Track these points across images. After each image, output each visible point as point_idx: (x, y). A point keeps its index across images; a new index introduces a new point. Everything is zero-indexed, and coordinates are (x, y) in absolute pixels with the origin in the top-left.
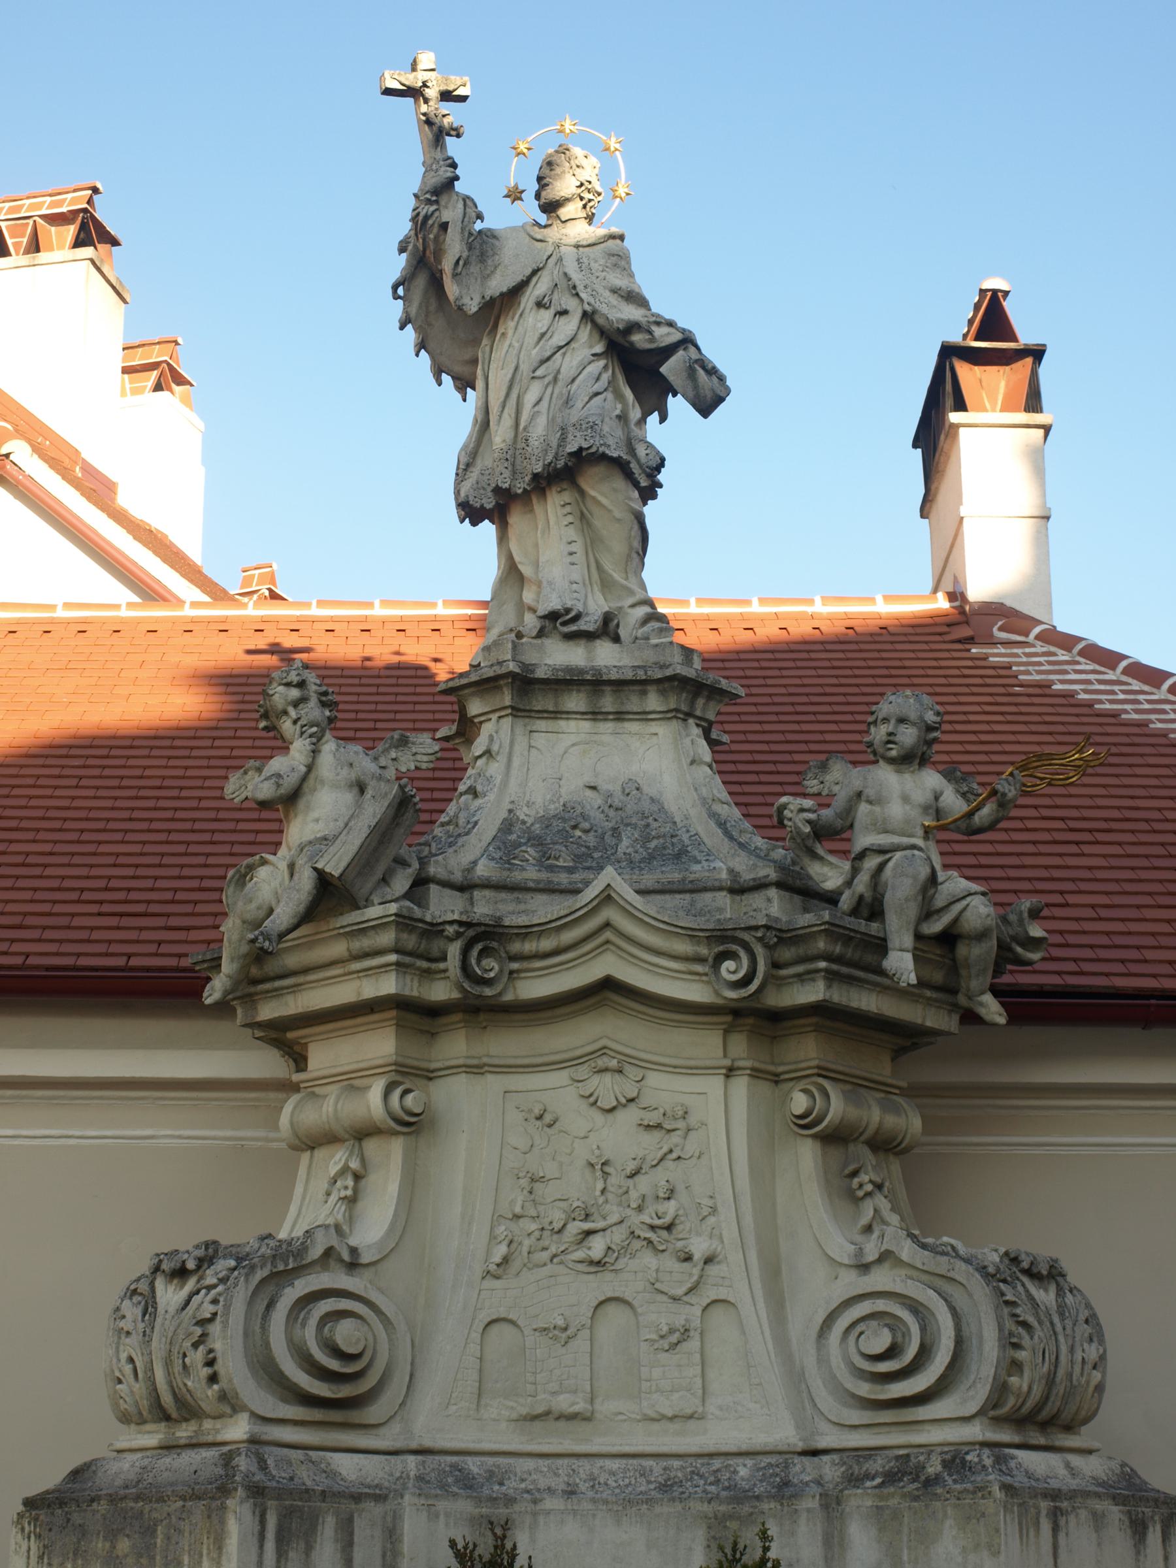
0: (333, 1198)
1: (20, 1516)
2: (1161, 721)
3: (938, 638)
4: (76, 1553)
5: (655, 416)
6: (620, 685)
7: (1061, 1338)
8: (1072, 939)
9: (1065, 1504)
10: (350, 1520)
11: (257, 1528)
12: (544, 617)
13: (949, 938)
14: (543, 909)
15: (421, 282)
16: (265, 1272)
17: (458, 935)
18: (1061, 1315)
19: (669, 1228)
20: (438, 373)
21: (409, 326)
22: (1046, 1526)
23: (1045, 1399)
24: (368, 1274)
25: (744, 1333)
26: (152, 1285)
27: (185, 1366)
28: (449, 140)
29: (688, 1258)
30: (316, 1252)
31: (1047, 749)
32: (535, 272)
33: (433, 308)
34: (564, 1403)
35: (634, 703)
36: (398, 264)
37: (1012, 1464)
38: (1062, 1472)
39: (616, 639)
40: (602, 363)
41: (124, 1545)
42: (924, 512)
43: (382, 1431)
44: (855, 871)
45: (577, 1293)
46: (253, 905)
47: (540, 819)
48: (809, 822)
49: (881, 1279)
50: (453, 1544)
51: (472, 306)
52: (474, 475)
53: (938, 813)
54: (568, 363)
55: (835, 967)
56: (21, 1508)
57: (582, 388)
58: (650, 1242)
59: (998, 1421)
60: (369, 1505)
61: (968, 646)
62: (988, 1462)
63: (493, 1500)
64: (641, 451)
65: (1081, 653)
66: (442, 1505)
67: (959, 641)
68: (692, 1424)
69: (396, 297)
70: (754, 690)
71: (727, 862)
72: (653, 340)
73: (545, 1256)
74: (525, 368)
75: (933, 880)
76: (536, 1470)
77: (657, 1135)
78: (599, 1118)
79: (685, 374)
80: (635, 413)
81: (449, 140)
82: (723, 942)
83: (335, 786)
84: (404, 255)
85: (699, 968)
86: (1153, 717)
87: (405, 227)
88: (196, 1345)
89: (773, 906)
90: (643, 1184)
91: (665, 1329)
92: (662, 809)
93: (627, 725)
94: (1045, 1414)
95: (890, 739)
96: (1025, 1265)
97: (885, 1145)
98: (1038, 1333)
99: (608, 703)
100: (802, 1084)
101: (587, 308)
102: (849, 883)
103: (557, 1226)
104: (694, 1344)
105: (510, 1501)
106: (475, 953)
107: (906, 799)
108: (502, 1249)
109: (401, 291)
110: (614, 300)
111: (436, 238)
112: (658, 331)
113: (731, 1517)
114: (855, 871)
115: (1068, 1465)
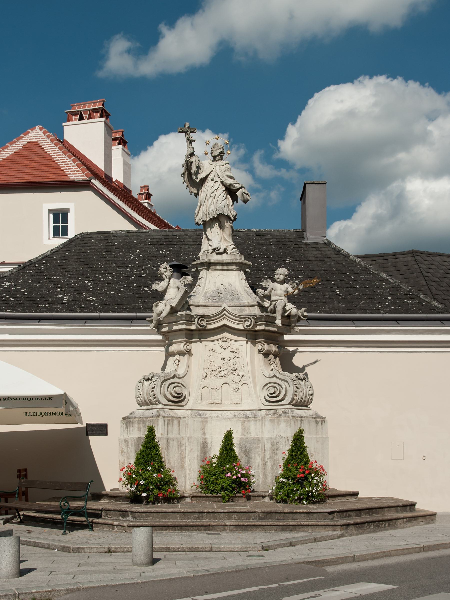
5: (236, 202)
13: (289, 316)
17: (197, 317)
22: (299, 422)
34: (217, 401)
35: (230, 267)
36: (183, 170)
39: (227, 254)
40: (224, 192)
42: (301, 200)
44: (271, 304)
45: (219, 382)
46: (158, 311)
47: (212, 291)
49: (274, 380)
53: (288, 292)
54: (218, 193)
57: (220, 199)
59: (293, 405)
62: (290, 412)
69: (182, 177)
73: (213, 375)
74: (209, 194)
83: (173, 288)
88: (152, 392)
89: (256, 311)
90: (231, 362)
92: (236, 289)
95: (278, 278)
100: (260, 344)
102: (270, 306)
104: (240, 391)
106: (200, 320)
107: (281, 290)
108: (206, 374)
110: (227, 178)
112: (236, 185)
114: (271, 304)
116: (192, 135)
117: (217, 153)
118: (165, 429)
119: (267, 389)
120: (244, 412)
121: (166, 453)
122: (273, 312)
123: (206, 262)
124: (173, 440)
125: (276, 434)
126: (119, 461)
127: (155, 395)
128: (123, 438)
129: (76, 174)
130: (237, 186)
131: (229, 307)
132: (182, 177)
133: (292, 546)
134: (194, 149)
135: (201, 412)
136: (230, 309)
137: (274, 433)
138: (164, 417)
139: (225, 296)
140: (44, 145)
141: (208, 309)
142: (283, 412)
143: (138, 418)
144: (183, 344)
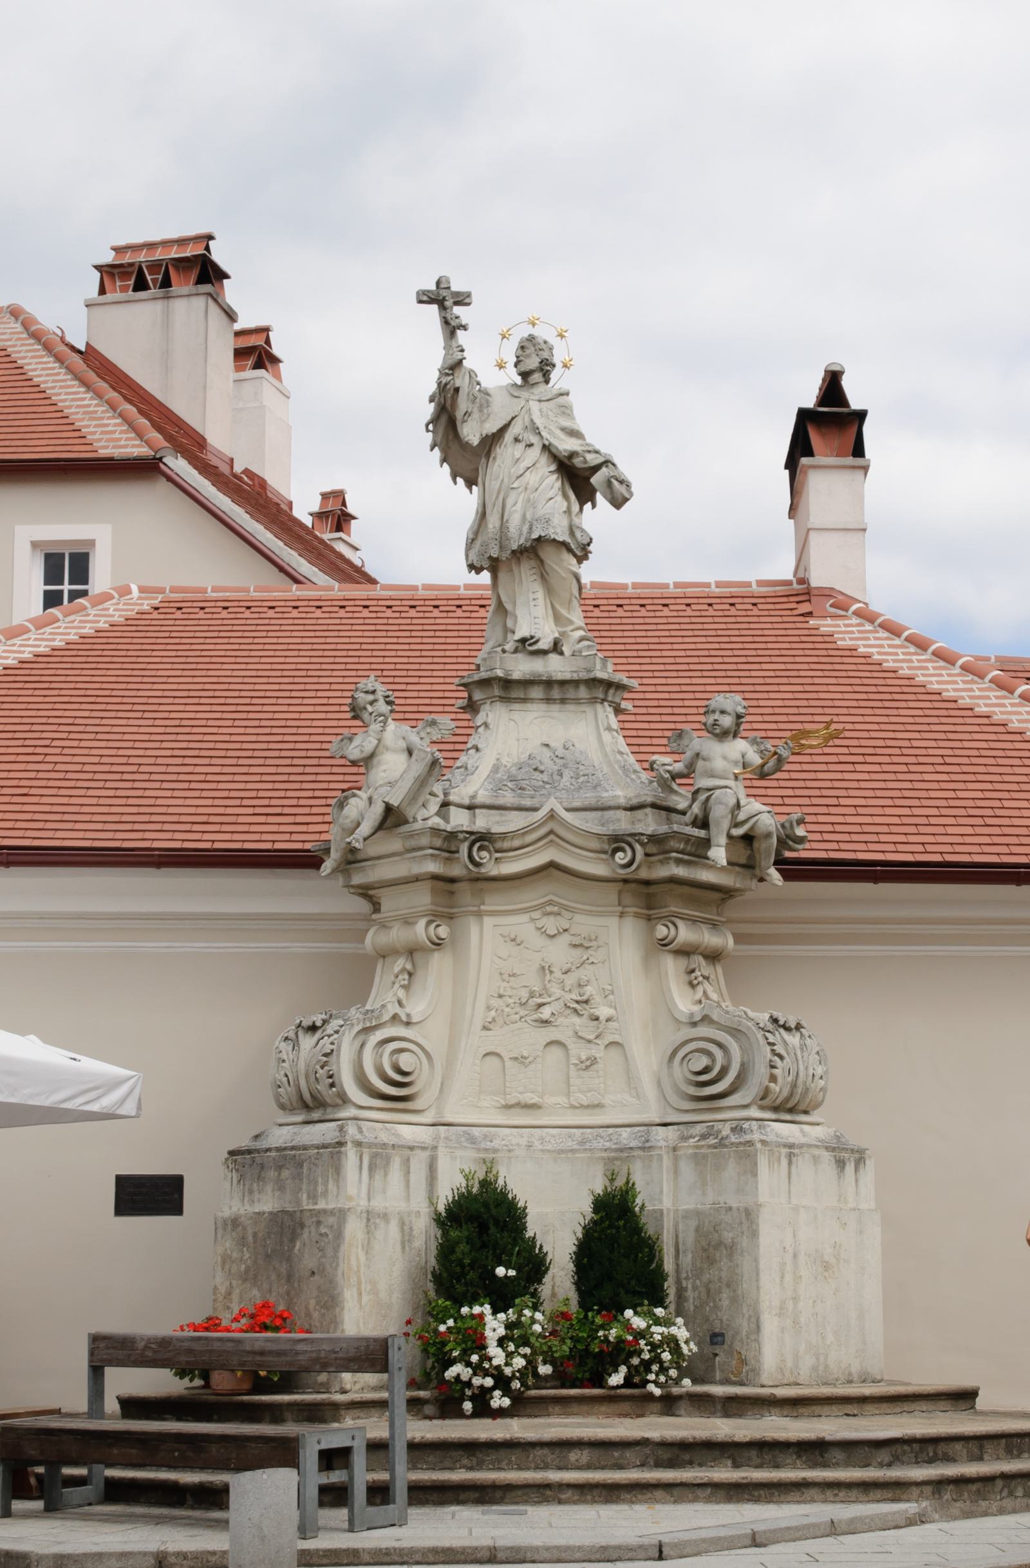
0: (397, 986)
1: (227, 1159)
2: (923, 675)
3: (789, 613)
4: (259, 1178)
5: (589, 505)
6: (563, 683)
7: (800, 1062)
8: (838, 828)
9: (796, 1151)
10: (408, 1160)
11: (358, 1163)
12: (518, 641)
14: (515, 822)
15: (444, 419)
16: (360, 1027)
17: (466, 839)
18: (802, 1049)
19: (586, 1002)
20: (454, 478)
21: (436, 448)
22: (784, 1162)
23: (791, 1094)
24: (417, 1028)
25: (626, 1059)
26: (296, 1034)
27: (316, 1079)
28: (459, 333)
29: (597, 1019)
30: (386, 1017)
31: (808, 727)
32: (513, 418)
33: (451, 437)
35: (571, 693)
36: (429, 409)
37: (768, 1129)
38: (798, 1134)
39: (562, 653)
41: (286, 1173)
43: (426, 1113)
44: (694, 800)
45: (531, 1039)
46: (348, 821)
47: (514, 765)
48: (668, 771)
50: (462, 1171)
51: (475, 441)
52: (477, 545)
54: (532, 478)
55: (680, 856)
56: (227, 1156)
58: (575, 1010)
60: (418, 1152)
61: (807, 619)
63: (486, 1150)
64: (578, 534)
65: (880, 625)
66: (458, 1153)
67: (802, 615)
68: (597, 1110)
69: (428, 431)
70: (645, 681)
71: (621, 794)
72: (585, 461)
73: (518, 1017)
75: (738, 806)
76: (511, 1134)
77: (579, 951)
78: (548, 942)
79: (605, 485)
80: (576, 507)
81: (459, 333)
82: (617, 842)
84: (433, 404)
85: (603, 856)
86: (919, 672)
87: (433, 387)
89: (649, 823)
90: (570, 980)
91: (584, 1058)
93: (567, 706)
94: (790, 1105)
96: (781, 1023)
97: (713, 956)
98: (787, 1059)
99: (556, 693)
101: (547, 443)
102: (690, 806)
103: (524, 1000)
105: (495, 1151)
109: (431, 427)
110: (562, 435)
111: (453, 396)
112: (589, 457)
113: (617, 1159)
115: (802, 1131)
116: (457, 310)
117: (533, 363)
118: (360, 1181)
119: (683, 1058)
120: (611, 1130)
121: (362, 1258)
122: (699, 823)
123: (499, 679)
124: (385, 1217)
125: (710, 1199)
126: (215, 1288)
127: (331, 1077)
128: (227, 1213)
129: (113, 437)
130: (592, 459)
131: (568, 810)
132: (428, 431)
133: (756, 1546)
134: (462, 351)
135: (476, 1131)
136: (568, 817)
137: (704, 1194)
138: (358, 1144)
139: (556, 777)
140: (25, 358)
141: (502, 815)
142: (733, 1130)
143: (278, 1149)
144: (422, 923)
